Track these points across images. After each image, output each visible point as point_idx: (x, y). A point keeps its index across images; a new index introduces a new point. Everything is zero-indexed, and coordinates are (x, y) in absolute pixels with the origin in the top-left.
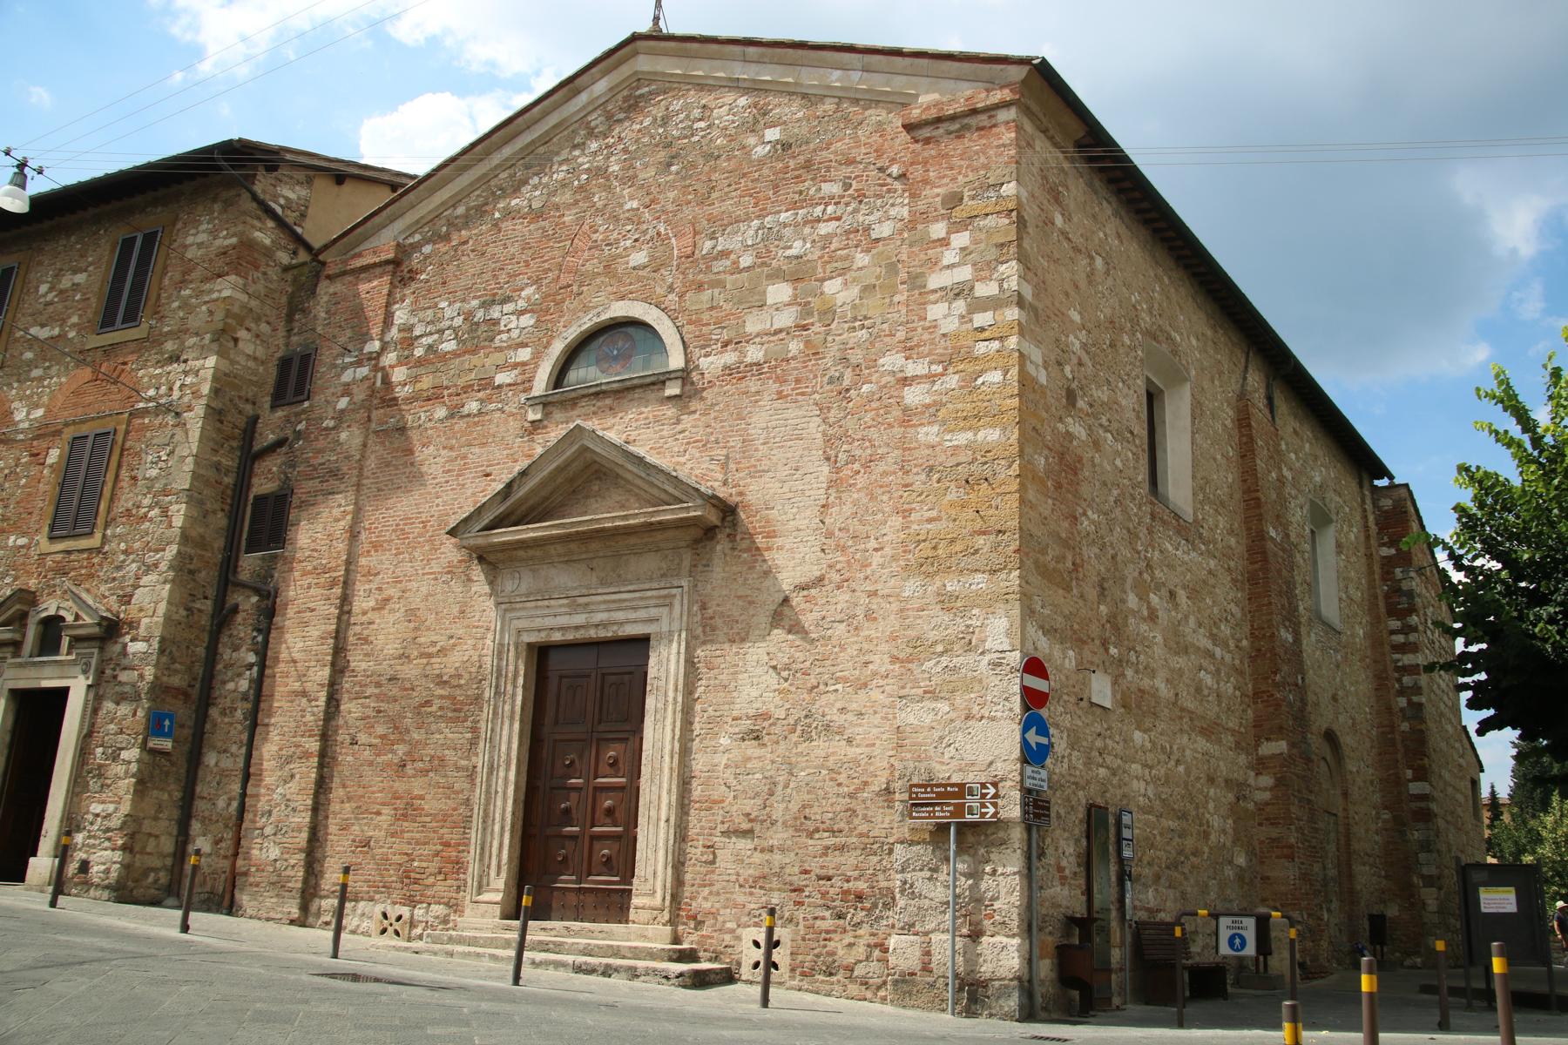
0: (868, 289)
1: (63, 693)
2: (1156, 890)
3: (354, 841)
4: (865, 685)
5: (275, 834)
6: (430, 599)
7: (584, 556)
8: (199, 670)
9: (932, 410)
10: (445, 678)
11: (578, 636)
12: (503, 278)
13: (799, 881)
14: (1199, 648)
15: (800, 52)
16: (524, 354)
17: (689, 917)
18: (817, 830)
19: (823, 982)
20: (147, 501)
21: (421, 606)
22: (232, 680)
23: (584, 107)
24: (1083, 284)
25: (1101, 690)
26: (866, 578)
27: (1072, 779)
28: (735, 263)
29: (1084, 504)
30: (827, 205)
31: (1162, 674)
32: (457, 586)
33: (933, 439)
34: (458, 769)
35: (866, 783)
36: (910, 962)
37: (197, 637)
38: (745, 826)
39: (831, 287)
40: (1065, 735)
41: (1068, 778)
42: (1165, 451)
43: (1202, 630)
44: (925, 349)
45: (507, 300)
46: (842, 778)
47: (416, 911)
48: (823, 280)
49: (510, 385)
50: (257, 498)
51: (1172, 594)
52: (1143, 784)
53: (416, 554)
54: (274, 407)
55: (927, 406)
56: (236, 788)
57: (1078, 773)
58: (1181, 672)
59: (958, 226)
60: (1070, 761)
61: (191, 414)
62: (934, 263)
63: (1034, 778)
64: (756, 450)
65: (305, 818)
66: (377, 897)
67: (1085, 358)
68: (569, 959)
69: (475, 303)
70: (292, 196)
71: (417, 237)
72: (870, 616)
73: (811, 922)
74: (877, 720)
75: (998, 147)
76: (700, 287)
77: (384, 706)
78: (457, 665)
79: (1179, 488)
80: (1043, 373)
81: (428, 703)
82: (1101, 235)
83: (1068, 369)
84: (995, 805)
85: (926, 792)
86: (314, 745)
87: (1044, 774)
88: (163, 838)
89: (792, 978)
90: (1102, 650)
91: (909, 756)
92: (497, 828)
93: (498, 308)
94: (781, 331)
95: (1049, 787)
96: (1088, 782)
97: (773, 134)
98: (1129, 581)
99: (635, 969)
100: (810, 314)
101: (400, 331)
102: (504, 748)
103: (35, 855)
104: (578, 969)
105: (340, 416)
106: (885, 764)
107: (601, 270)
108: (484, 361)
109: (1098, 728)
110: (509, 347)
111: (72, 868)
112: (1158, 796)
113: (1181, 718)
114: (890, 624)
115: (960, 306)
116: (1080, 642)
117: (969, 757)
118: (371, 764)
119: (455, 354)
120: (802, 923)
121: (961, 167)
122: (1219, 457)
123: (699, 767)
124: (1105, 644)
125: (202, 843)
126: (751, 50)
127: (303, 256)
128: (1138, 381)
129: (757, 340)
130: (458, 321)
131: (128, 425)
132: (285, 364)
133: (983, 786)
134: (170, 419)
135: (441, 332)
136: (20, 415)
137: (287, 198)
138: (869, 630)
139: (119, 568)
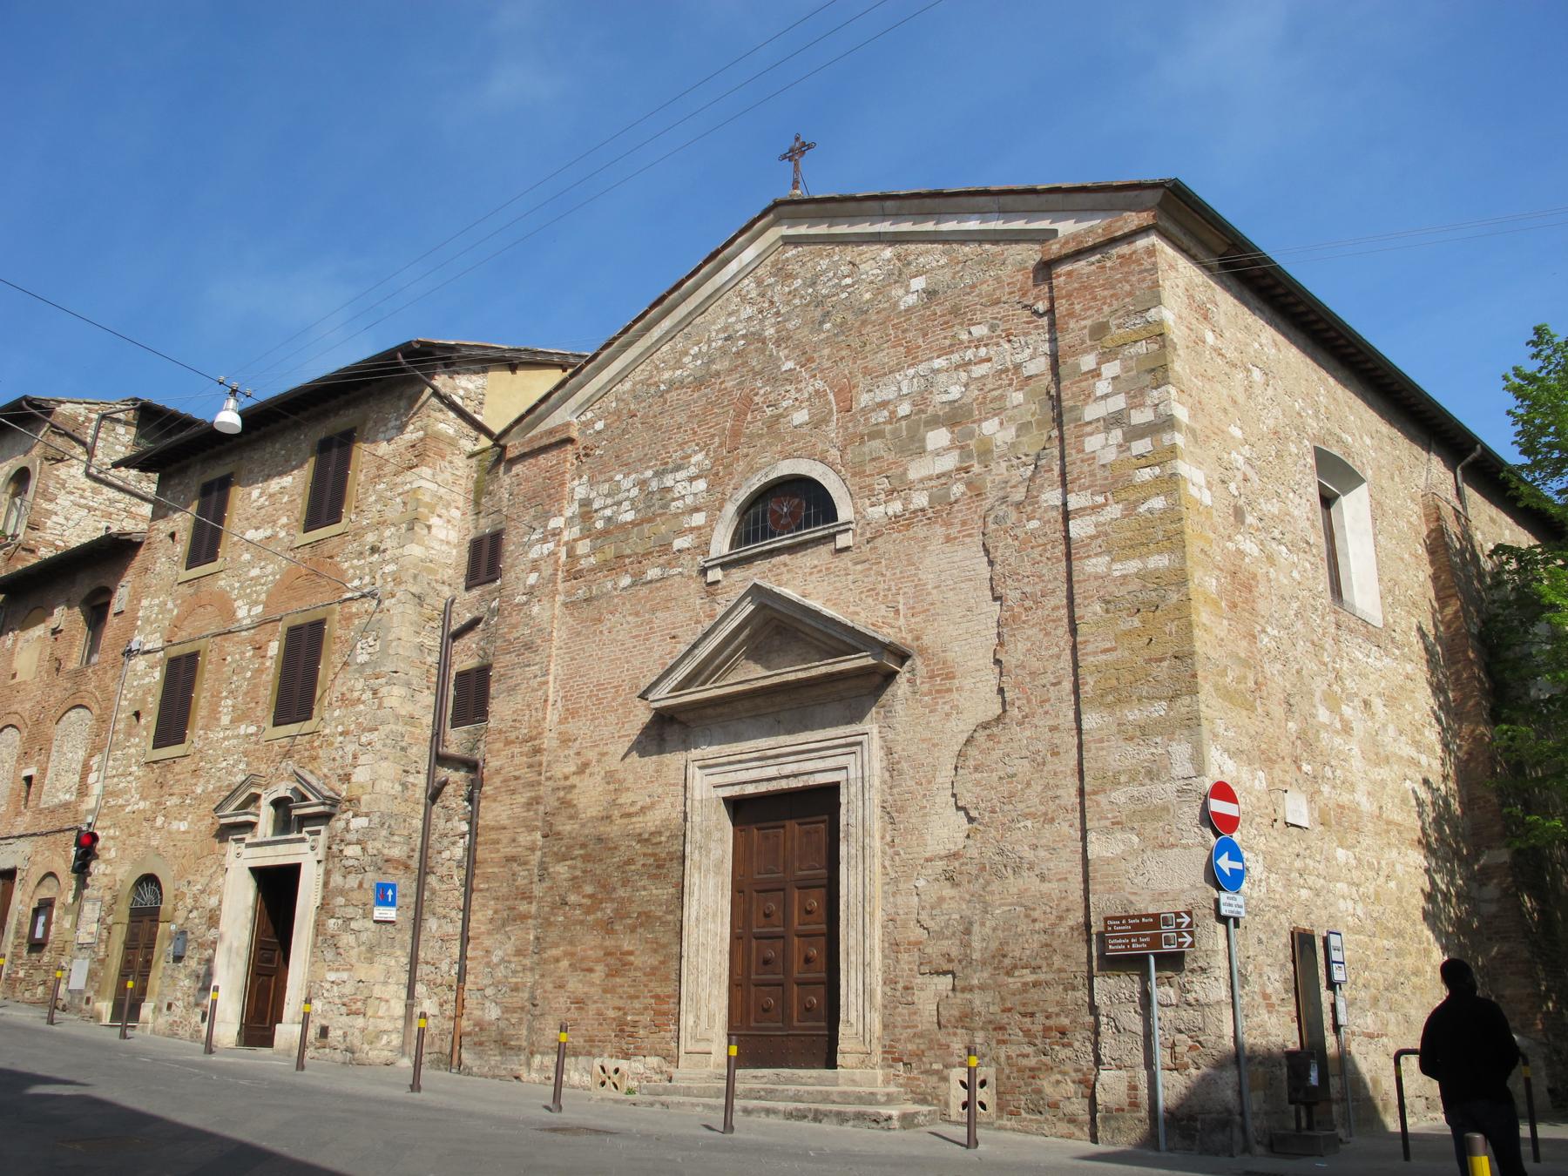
2: (1375, 1014)
7: (770, 710)
8: (417, 841)
11: (771, 788)
14: (1402, 757)
15: (937, 201)
18: (1015, 967)
22: (447, 848)
23: (735, 276)
24: (1241, 398)
25: (1297, 808)
27: (1272, 903)
28: (893, 413)
29: (1262, 622)
30: (977, 347)
31: (1362, 788)
33: (1102, 569)
37: (413, 810)
39: (990, 427)
40: (1260, 858)
41: (1267, 902)
42: (1346, 556)
43: (1403, 738)
45: (678, 468)
46: (1036, 914)
48: (980, 420)
50: (459, 675)
51: (1366, 704)
52: (1350, 904)
54: (468, 588)
56: (456, 951)
57: (1277, 896)
58: (1383, 782)
59: (1107, 356)
60: (1268, 884)
62: (1088, 396)
63: (1230, 905)
64: (929, 594)
67: (1251, 474)
68: (781, 1105)
69: (649, 473)
70: (471, 386)
71: (589, 415)
75: (1141, 272)
77: (589, 866)
78: (657, 823)
79: (1364, 592)
80: (1207, 493)
81: (630, 861)
82: (1256, 345)
83: (1232, 487)
84: (1191, 934)
85: (1121, 925)
87: (1240, 900)
88: (393, 1002)
89: (1000, 1117)
90: (1294, 767)
93: (670, 476)
94: (943, 475)
95: (1247, 912)
96: (1290, 906)
98: (1318, 694)
100: (970, 456)
101: (580, 506)
103: (280, 1022)
104: (789, 1115)
105: (530, 592)
109: (1296, 848)
110: (683, 513)
111: (312, 1033)
112: (1369, 915)
113: (1388, 831)
115: (1117, 435)
116: (1268, 760)
118: (582, 922)
121: (1105, 298)
122: (1406, 556)
124: (1296, 761)
125: (428, 1005)
126: (889, 204)
127: (486, 442)
128: (1310, 489)
132: (476, 546)
133: (1178, 915)
135: (619, 503)
136: (241, 613)
137: (466, 389)
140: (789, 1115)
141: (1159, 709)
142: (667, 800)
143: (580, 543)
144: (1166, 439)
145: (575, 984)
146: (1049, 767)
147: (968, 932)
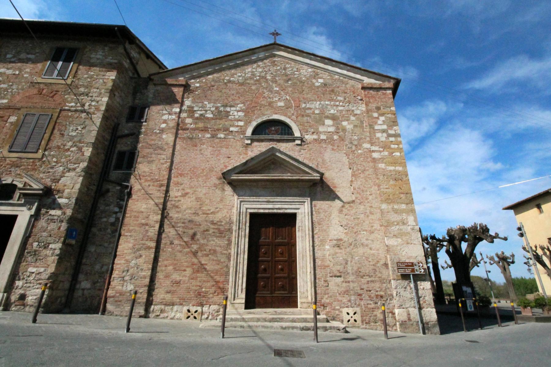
0: (355, 126)
1: (13, 218)
3: (172, 281)
4: (373, 232)
5: (131, 279)
6: (207, 195)
9: (382, 160)
10: (215, 222)
12: (230, 99)
13: (360, 292)
16: (241, 123)
17: (321, 305)
18: (364, 276)
19: (374, 325)
20: (70, 144)
21: (203, 197)
26: (368, 202)
32: (218, 192)
34: (222, 254)
35: (378, 262)
36: (404, 318)
38: (338, 274)
44: (377, 144)
46: (370, 260)
47: (204, 308)
48: (342, 121)
49: (236, 132)
53: (200, 179)
55: (380, 159)
61: (95, 116)
65: (149, 273)
66: (184, 303)
72: (371, 213)
73: (366, 305)
74: (378, 243)
76: (303, 116)
77: (186, 230)
78: (220, 218)
81: (207, 230)
86: (153, 244)
89: (363, 324)
91: (392, 253)
92: (241, 275)
97: (321, 81)
99: (326, 327)
102: (242, 247)
106: (383, 256)
107: (268, 104)
108: (221, 123)
114: (378, 215)
115: (385, 135)
117: (410, 255)
118: (181, 252)
119: (212, 119)
120: (363, 306)
123: (319, 255)
129: (323, 133)
130: (213, 109)
131: (59, 114)
134: (83, 115)
138: (371, 217)
139: (52, 168)
140: (303, 329)
141: (404, 206)
142: (225, 210)
143: (187, 119)
144: (399, 139)
145: (176, 276)
146: (370, 218)
147: (346, 264)
